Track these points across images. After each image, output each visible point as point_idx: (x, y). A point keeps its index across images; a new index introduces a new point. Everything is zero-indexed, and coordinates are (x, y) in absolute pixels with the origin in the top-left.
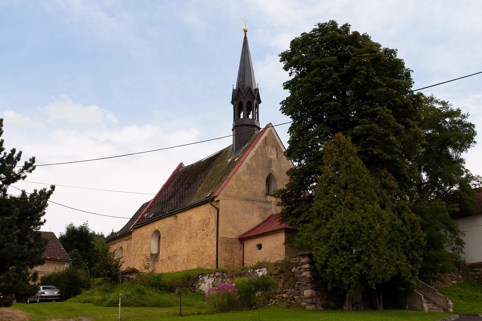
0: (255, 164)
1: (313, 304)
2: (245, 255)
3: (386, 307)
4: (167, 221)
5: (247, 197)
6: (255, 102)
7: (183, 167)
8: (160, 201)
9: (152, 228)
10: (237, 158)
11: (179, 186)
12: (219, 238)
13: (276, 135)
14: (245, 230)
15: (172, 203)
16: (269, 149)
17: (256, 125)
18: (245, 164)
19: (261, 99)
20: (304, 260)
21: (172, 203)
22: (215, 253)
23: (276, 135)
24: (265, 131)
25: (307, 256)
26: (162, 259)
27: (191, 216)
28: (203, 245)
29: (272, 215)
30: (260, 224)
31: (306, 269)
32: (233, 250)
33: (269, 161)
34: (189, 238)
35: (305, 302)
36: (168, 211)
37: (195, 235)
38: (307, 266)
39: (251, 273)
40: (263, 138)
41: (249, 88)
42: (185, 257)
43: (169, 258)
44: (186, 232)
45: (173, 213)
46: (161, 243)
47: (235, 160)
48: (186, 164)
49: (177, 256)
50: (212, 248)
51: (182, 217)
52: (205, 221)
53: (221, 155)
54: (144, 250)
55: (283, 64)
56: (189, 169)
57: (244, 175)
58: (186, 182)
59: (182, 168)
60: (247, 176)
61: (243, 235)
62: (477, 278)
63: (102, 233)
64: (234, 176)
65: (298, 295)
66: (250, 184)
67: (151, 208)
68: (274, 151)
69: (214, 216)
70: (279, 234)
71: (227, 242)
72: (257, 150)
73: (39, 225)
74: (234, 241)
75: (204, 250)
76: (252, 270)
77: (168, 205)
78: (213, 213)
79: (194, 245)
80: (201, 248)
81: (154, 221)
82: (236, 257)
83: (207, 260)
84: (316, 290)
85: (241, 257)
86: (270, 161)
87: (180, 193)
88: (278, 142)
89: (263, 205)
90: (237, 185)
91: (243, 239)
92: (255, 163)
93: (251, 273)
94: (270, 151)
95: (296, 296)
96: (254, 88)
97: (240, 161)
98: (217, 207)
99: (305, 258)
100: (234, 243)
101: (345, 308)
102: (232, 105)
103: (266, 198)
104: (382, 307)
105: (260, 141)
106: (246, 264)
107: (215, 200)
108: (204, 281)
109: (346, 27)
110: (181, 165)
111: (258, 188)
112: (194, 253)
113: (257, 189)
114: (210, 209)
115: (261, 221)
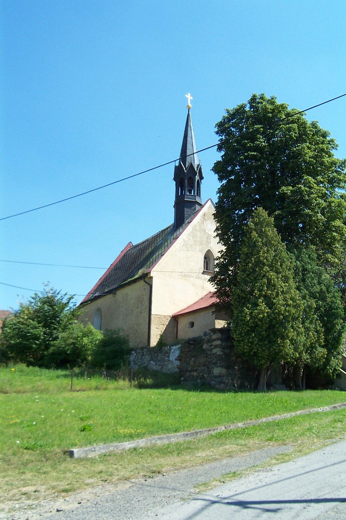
6: (197, 178)
17: (197, 202)
19: (203, 175)
31: (216, 346)
38: (218, 342)
48: (134, 244)
55: (216, 130)
76: (168, 347)
78: (146, 290)
92: (193, 239)
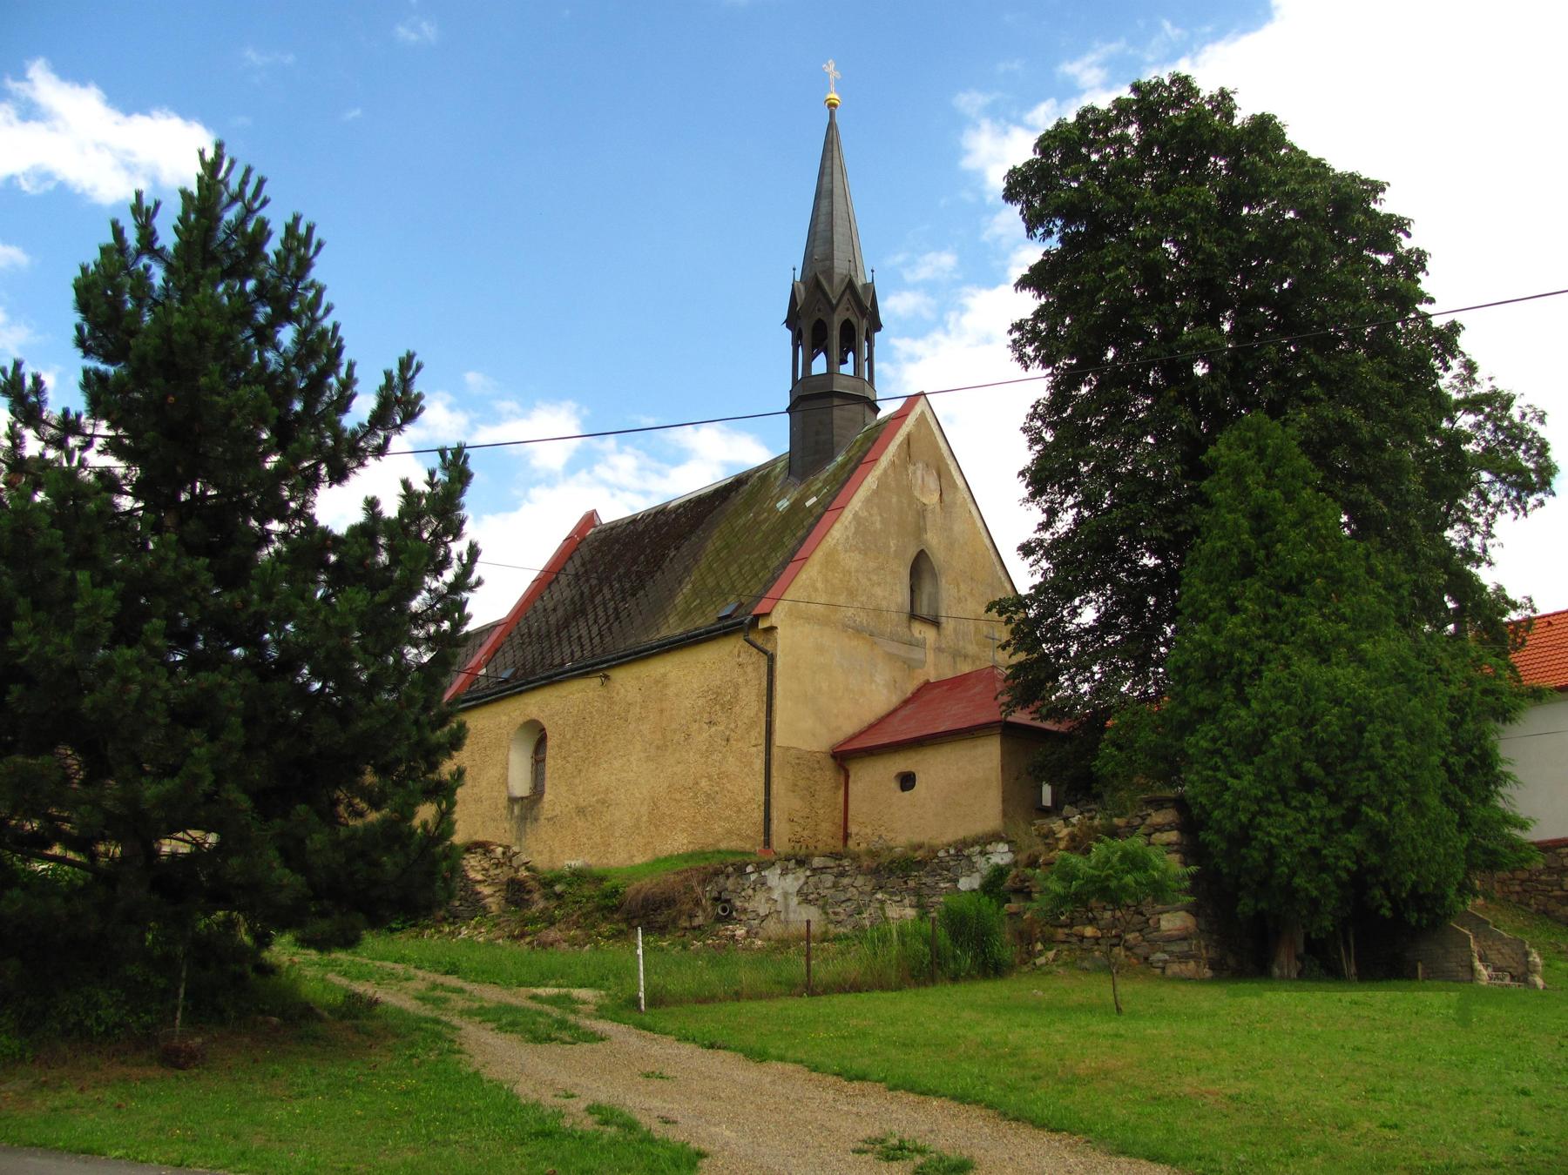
0: (879, 518)
1: (1193, 957)
2: (851, 806)
3: (1303, 975)
4: (571, 693)
5: (855, 621)
7: (598, 523)
8: (529, 628)
9: (514, 715)
10: (814, 499)
11: (594, 582)
12: (775, 751)
13: (937, 433)
14: (849, 727)
15: (580, 638)
16: (919, 473)
18: (851, 516)
20: (1158, 818)
21: (580, 638)
22: (762, 798)
23: (937, 433)
24: (907, 415)
25: (1170, 805)
26: (554, 814)
27: (664, 675)
28: (714, 771)
29: (927, 683)
30: (892, 708)
32: (815, 790)
33: (918, 513)
34: (658, 748)
35: (1165, 952)
36: (572, 660)
37: (679, 737)
38: (1173, 836)
39: (948, 859)
40: (900, 437)
41: (847, 280)
42: (644, 810)
43: (581, 811)
44: (645, 728)
45: (598, 665)
46: (549, 762)
47: (808, 504)
49: (610, 805)
50: (748, 780)
51: (628, 681)
52: (718, 694)
53: (741, 490)
54: (484, 784)
56: (624, 530)
57: (846, 551)
58: (621, 570)
59: (595, 526)
60: (857, 556)
61: (844, 743)
62: (1518, 888)
63: (1490, 564)
64: (818, 556)
65: (1139, 927)
66: (864, 581)
67: (497, 650)
68: (932, 482)
69: (756, 677)
70: (979, 742)
71: (799, 764)
72: (885, 471)
73: (1040, 542)
74: (819, 762)
75: (717, 789)
77: (565, 643)
78: (749, 669)
79: (678, 769)
80: (704, 780)
81: (521, 693)
82: (822, 811)
83: (727, 819)
84: (1196, 915)
85: (839, 815)
86: (922, 512)
87: (605, 604)
88: (942, 455)
89: (902, 651)
90: (827, 581)
91: (845, 757)
93: (948, 859)
94: (920, 481)
95: (1133, 931)
96: (859, 282)
97: (831, 505)
98: (769, 648)
99: (1164, 811)
100: (817, 766)
101: (1276, 971)
102: (789, 333)
103: (909, 627)
104: (1353, 970)
105: (892, 448)
106: (857, 834)
107: (763, 625)
108: (763, 884)
109: (1224, 101)
110: (590, 518)
111: (887, 594)
112: (678, 796)
113: (884, 598)
114: (739, 656)
115: (895, 700)
